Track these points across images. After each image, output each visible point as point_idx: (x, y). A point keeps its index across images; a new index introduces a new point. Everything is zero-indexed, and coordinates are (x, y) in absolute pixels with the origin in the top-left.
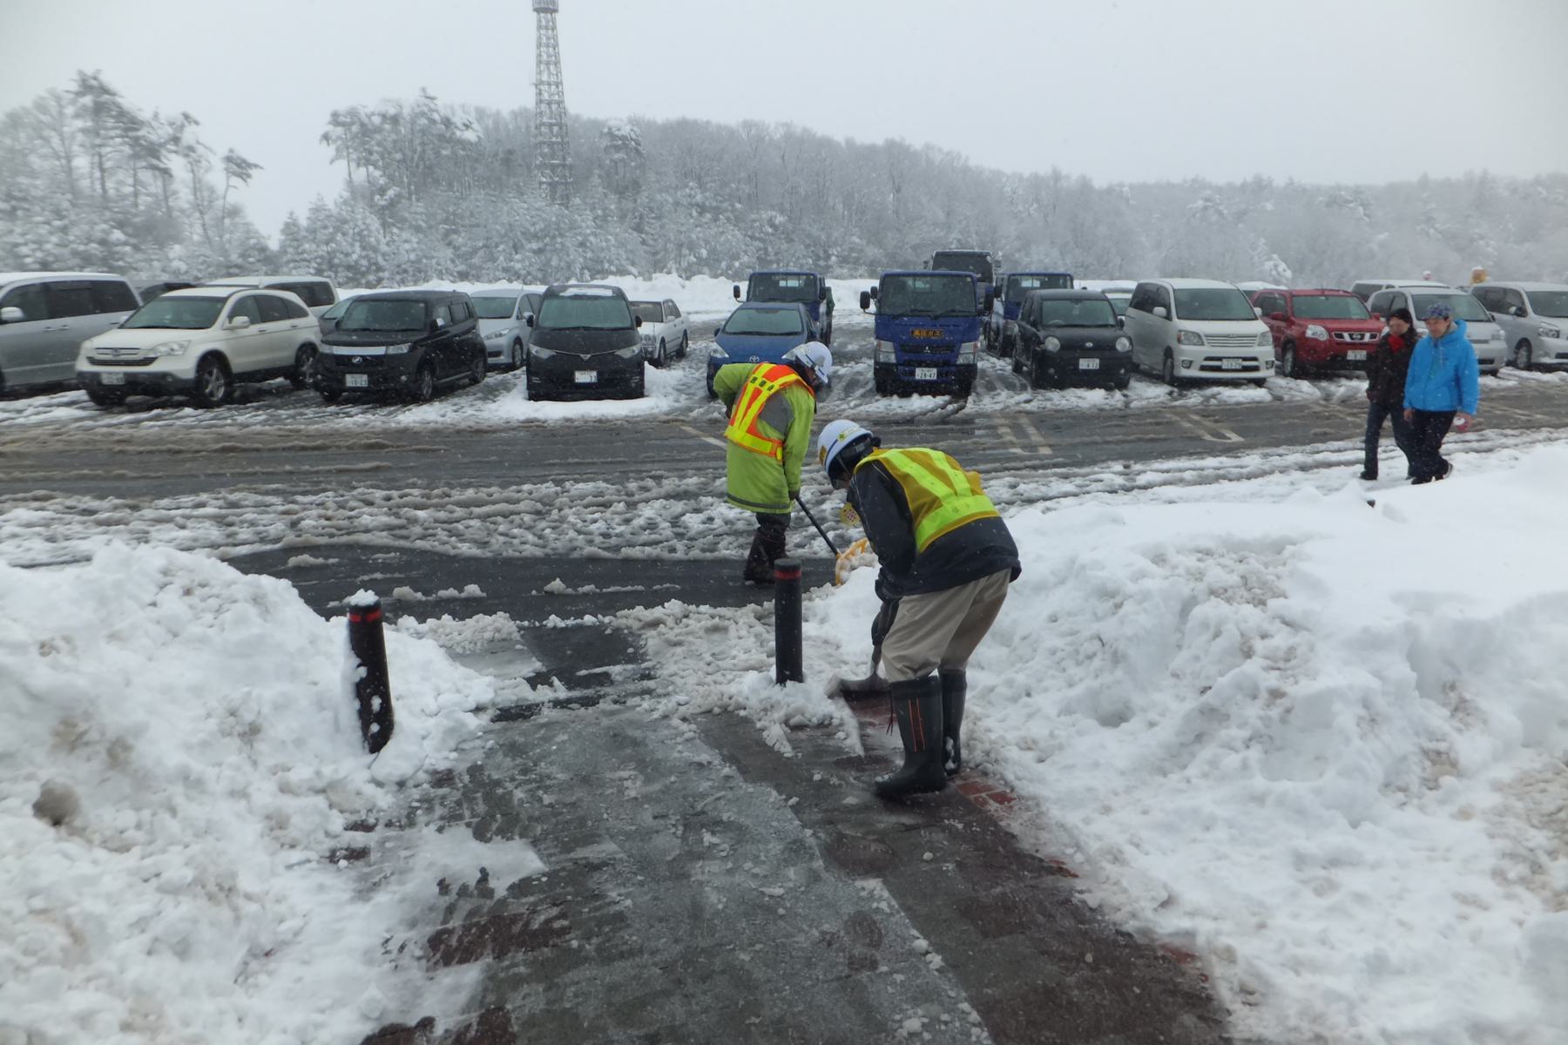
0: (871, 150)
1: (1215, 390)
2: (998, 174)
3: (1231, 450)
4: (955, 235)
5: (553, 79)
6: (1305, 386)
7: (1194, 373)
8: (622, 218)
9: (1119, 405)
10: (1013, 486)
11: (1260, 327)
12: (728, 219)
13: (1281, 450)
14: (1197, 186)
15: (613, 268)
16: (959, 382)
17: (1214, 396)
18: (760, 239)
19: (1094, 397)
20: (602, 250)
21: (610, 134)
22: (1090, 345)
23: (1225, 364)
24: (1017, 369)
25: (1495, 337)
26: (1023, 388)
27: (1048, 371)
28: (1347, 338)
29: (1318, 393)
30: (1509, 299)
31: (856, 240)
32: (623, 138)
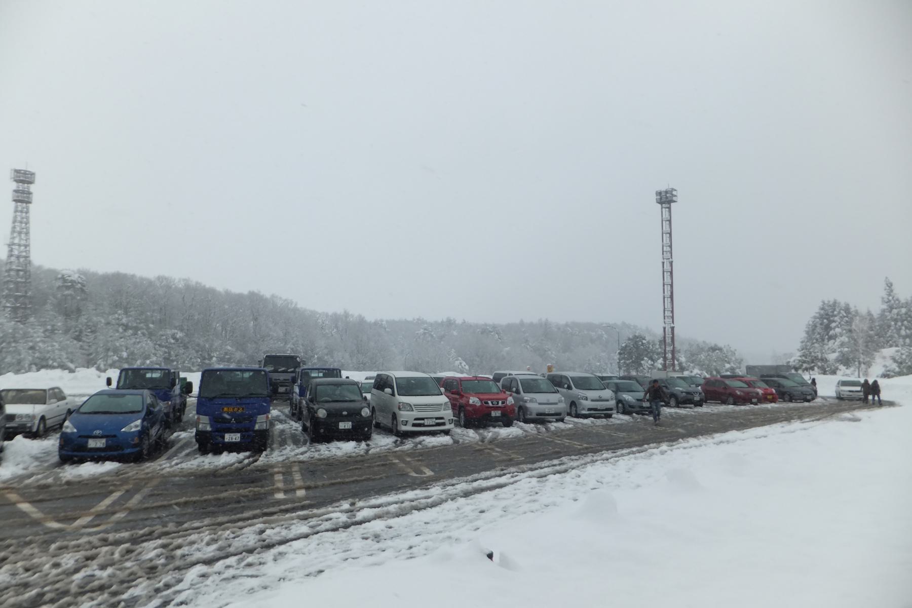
0: (240, 296)
1: (422, 438)
2: (313, 313)
3: (424, 484)
4: (289, 346)
5: (23, 242)
6: (471, 433)
7: (409, 428)
8: (66, 331)
9: (362, 453)
10: (262, 532)
11: (443, 399)
12: (144, 334)
13: (454, 481)
14: (420, 322)
15: (55, 364)
16: (257, 442)
17: (420, 443)
18: (166, 347)
19: (348, 447)
20: (48, 352)
21: (63, 279)
22: (345, 413)
23: (426, 422)
24: (305, 429)
25: (560, 401)
26: (305, 443)
27: (321, 432)
28: (490, 404)
29: (478, 437)
30: (564, 381)
31: (229, 348)
32: (72, 281)
